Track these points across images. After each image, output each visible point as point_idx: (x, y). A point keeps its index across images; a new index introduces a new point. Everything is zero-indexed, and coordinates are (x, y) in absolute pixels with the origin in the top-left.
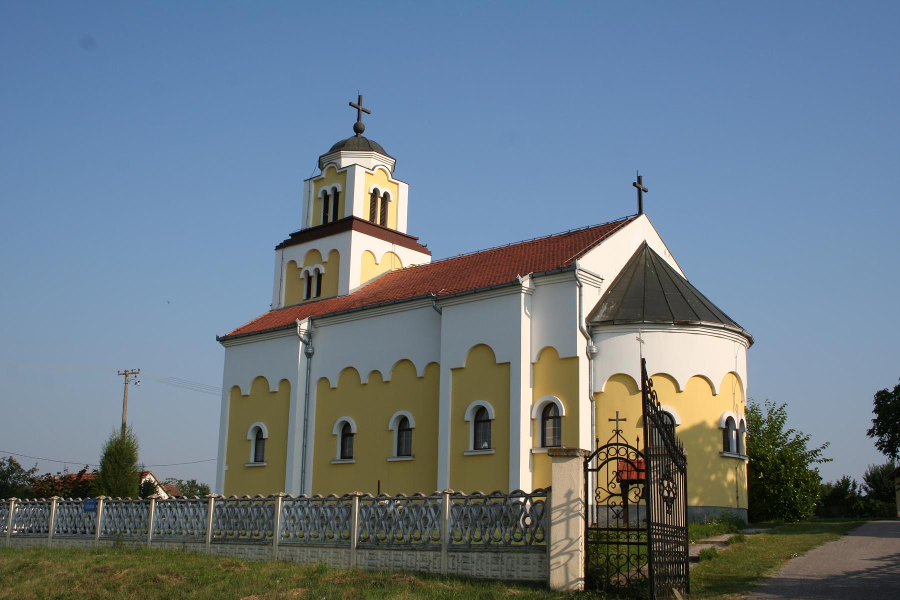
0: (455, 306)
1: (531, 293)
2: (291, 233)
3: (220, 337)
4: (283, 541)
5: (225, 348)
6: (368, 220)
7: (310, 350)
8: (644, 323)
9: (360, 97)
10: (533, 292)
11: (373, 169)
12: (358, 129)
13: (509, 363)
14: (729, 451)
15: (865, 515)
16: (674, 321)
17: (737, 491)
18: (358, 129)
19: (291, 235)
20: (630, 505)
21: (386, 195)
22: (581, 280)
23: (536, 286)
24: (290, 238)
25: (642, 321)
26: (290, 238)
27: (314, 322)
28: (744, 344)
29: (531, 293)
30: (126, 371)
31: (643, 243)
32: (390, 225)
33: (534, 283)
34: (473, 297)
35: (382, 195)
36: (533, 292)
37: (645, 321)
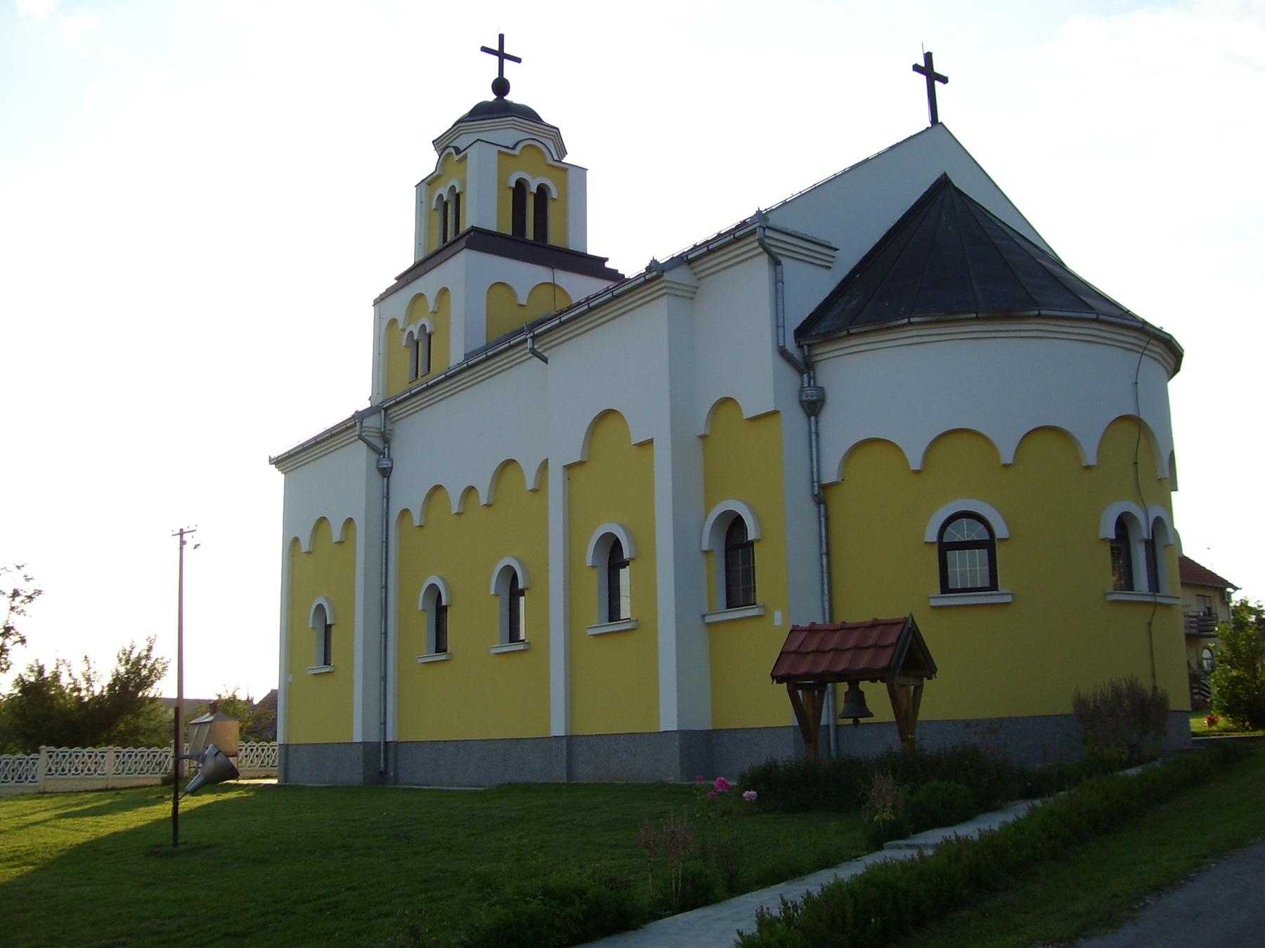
0: (565, 344)
1: (691, 295)
2: (396, 276)
3: (273, 457)
4: (1226, 730)
5: (283, 475)
6: (510, 232)
7: (385, 464)
8: (910, 323)
9: (501, 37)
10: (694, 293)
11: (514, 148)
12: (501, 86)
13: (651, 441)
14: (1133, 590)
15: (30, 867)
16: (977, 313)
17: (1153, 675)
18: (501, 86)
19: (396, 279)
20: (363, 738)
21: (542, 192)
22: (774, 250)
23: (699, 279)
24: (396, 281)
25: (906, 320)
26: (396, 281)
27: (389, 412)
28: (553, 138)
29: (691, 295)
30: (181, 530)
31: (942, 176)
32: (553, 239)
33: (695, 274)
34: (594, 318)
35: (534, 190)
36: (694, 293)
37: (912, 320)
